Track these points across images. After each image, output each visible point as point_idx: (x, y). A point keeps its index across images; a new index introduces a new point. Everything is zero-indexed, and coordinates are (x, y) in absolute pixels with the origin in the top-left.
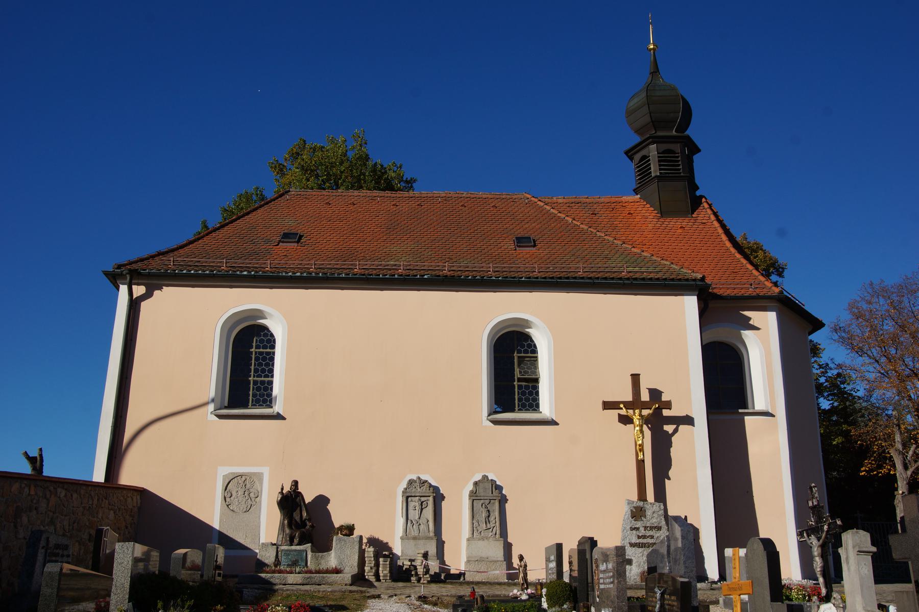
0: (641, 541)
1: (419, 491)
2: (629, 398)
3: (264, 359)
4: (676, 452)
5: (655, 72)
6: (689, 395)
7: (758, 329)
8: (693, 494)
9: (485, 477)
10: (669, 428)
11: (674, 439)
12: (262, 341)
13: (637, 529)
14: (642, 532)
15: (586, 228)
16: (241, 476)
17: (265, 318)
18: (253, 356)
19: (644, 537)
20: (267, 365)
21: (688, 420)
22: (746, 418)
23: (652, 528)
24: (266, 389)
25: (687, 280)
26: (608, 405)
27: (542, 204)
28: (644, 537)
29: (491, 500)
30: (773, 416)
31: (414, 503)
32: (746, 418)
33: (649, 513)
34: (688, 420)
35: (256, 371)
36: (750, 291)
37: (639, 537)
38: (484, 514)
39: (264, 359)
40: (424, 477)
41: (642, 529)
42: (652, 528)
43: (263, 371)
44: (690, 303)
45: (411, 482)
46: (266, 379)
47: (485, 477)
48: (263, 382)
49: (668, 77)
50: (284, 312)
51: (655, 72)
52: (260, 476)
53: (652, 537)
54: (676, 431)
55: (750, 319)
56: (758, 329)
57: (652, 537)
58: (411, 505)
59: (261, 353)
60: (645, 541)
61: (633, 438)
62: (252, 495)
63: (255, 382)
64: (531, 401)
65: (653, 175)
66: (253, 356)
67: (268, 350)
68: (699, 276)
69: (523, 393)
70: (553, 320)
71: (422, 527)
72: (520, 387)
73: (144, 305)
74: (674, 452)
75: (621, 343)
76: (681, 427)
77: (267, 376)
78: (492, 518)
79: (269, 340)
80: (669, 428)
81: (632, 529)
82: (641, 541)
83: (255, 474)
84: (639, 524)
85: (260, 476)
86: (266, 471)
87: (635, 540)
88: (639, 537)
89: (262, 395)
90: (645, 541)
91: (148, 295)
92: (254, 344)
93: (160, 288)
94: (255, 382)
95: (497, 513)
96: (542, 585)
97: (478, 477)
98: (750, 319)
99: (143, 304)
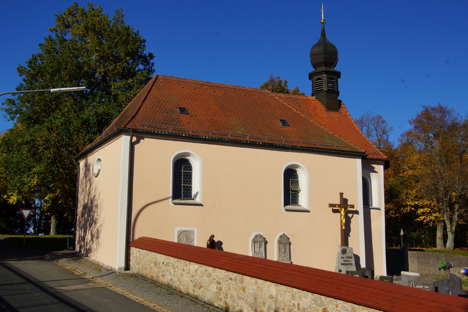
0: (345, 262)
1: (259, 239)
2: (138, 234)
3: (187, 175)
4: (352, 225)
5: (323, 35)
6: (357, 202)
7: (377, 172)
8: (357, 244)
9: (284, 234)
10: (350, 215)
11: (352, 220)
12: (186, 167)
13: (344, 258)
14: (345, 259)
15: (304, 116)
16: (185, 231)
17: (189, 156)
18: (183, 174)
19: (346, 261)
20: (189, 178)
21: (357, 212)
22: (371, 210)
23: (349, 257)
24: (189, 190)
25: (359, 152)
26: (331, 205)
27: (278, 98)
28: (346, 261)
29: (285, 242)
30: (309, 211)
31: (257, 245)
32: (371, 210)
33: (348, 251)
34: (357, 212)
35: (184, 181)
36: (375, 157)
37: (344, 261)
38: (283, 250)
39: (187, 175)
40: (261, 234)
41: (345, 258)
42: (349, 257)
43: (187, 181)
44: (359, 162)
45: (256, 236)
46: (189, 185)
47: (284, 234)
48: (187, 187)
49: (330, 38)
50: (201, 156)
51: (323, 35)
52: (193, 232)
53: (349, 261)
54: (352, 216)
55: (374, 168)
56: (377, 172)
57: (349, 261)
58: (256, 245)
59: (186, 173)
60: (346, 263)
61: (337, 220)
62: (190, 240)
63: (184, 186)
64: (295, 202)
65: (324, 90)
66: (183, 174)
67: (189, 171)
68: (364, 151)
69: (185, 190)
70: (310, 167)
71: (260, 255)
72: (292, 194)
73: (136, 146)
74: (352, 225)
75: (329, 177)
76: (355, 215)
77: (189, 184)
78: (286, 252)
79: (189, 167)
80: (350, 215)
81: (342, 258)
82: (345, 262)
83: (191, 231)
84: (344, 256)
85: (193, 232)
86: (195, 230)
87: (343, 262)
88: (344, 261)
89: (187, 193)
90: (346, 263)
91: (138, 142)
92: (183, 168)
93: (143, 139)
94: (184, 186)
95: (288, 250)
96: (418, 262)
97: (281, 234)
98: (374, 168)
99: (135, 146)
